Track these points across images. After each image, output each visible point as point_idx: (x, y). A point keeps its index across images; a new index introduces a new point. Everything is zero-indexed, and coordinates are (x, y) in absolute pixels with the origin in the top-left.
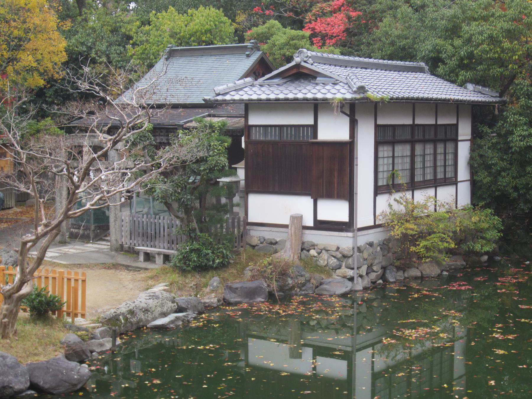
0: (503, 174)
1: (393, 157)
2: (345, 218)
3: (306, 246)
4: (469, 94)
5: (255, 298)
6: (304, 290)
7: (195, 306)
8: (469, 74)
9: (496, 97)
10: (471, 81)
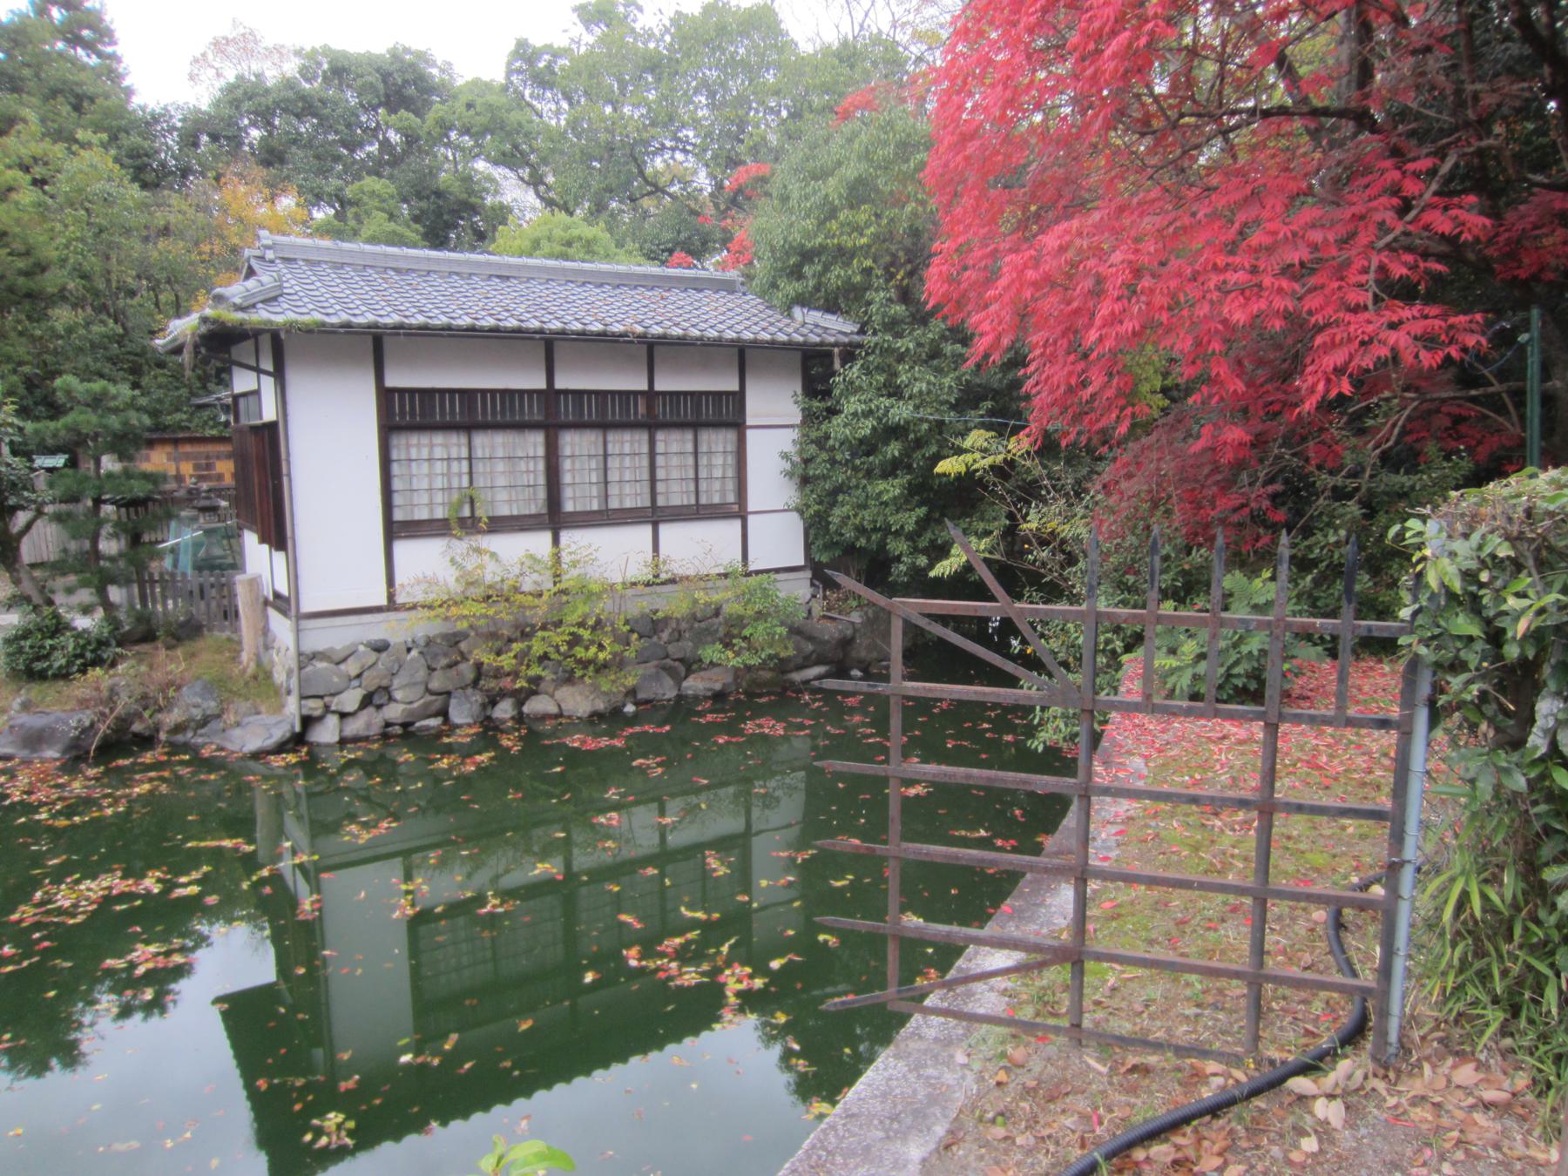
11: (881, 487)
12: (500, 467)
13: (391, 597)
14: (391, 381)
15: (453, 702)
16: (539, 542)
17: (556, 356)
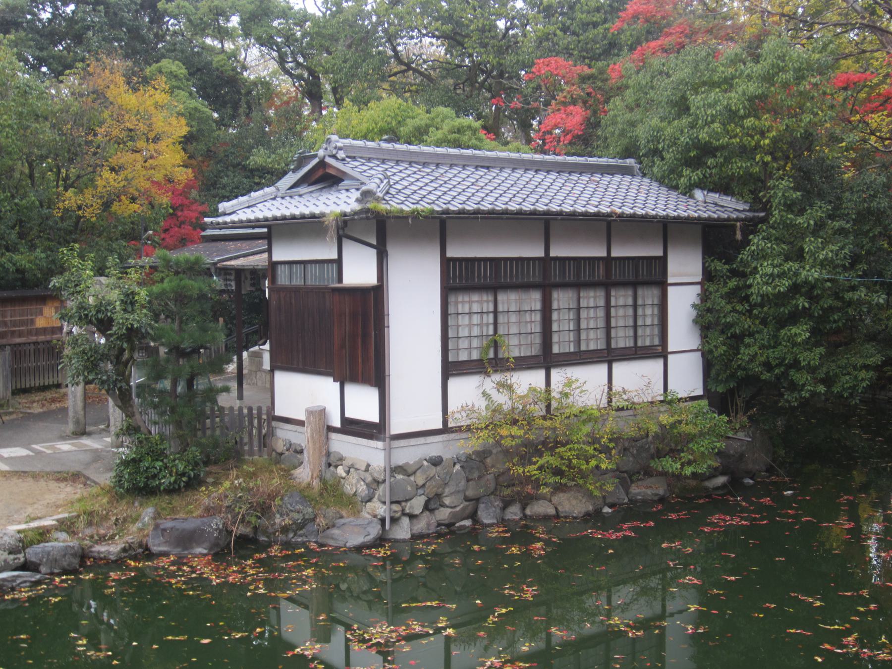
0: (747, 340)
1: (496, 312)
2: (375, 418)
3: (332, 459)
4: (703, 205)
5: (192, 548)
6: (301, 536)
7: (56, 560)
8: (696, 175)
9: (744, 210)
10: (701, 185)
11: (793, 331)
12: (513, 318)
13: (445, 422)
14: (451, 253)
15: (482, 506)
16: (534, 379)
17: (551, 232)
